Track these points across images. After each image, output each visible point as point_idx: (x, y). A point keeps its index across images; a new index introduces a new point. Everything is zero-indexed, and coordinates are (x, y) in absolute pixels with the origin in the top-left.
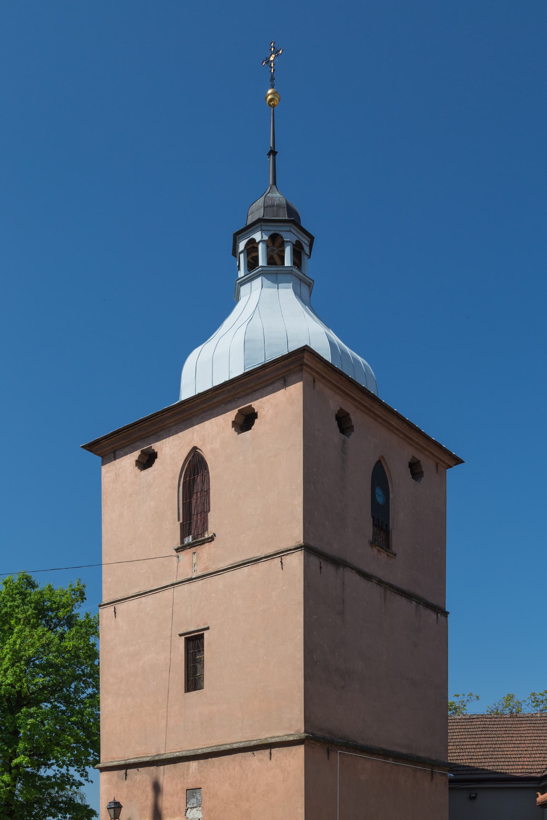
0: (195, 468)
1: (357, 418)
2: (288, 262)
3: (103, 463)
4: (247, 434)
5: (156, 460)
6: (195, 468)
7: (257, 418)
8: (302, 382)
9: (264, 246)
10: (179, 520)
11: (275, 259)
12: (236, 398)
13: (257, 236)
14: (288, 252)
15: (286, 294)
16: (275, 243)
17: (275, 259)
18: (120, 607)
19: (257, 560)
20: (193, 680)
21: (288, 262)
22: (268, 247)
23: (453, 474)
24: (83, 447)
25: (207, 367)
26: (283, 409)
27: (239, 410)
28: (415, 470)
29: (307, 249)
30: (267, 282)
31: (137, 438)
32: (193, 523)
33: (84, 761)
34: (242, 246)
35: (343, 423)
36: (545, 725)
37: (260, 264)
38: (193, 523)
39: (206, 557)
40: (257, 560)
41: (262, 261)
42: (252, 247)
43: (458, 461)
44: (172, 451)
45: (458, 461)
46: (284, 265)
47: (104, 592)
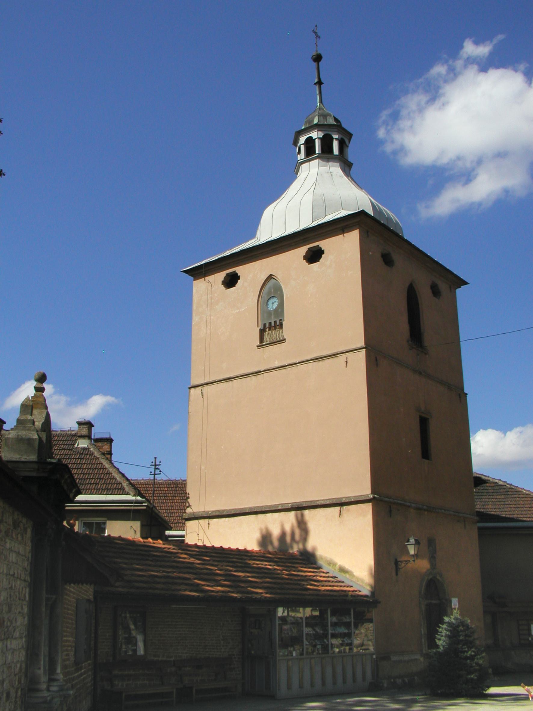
0: (271, 288)
1: (397, 257)
2: (336, 151)
3: (194, 280)
4: (315, 265)
5: (239, 281)
6: (271, 288)
7: (324, 254)
8: (358, 230)
9: (320, 141)
10: (258, 326)
11: (327, 149)
12: (309, 241)
14: (335, 144)
15: (336, 169)
16: (327, 142)
17: (327, 149)
18: (206, 389)
19: (258, 373)
20: (426, 454)
21: (336, 151)
23: (460, 292)
25: (281, 218)
26: (345, 249)
27: (253, 235)
28: (436, 291)
30: (322, 163)
31: (227, 268)
32: (271, 328)
33: (74, 491)
34: (302, 140)
35: (387, 260)
36: (530, 509)
37: (317, 152)
38: (271, 328)
39: (274, 355)
40: (258, 373)
41: (318, 150)
42: (310, 142)
43: (465, 283)
44: (252, 274)
45: (465, 283)
47: (193, 375)
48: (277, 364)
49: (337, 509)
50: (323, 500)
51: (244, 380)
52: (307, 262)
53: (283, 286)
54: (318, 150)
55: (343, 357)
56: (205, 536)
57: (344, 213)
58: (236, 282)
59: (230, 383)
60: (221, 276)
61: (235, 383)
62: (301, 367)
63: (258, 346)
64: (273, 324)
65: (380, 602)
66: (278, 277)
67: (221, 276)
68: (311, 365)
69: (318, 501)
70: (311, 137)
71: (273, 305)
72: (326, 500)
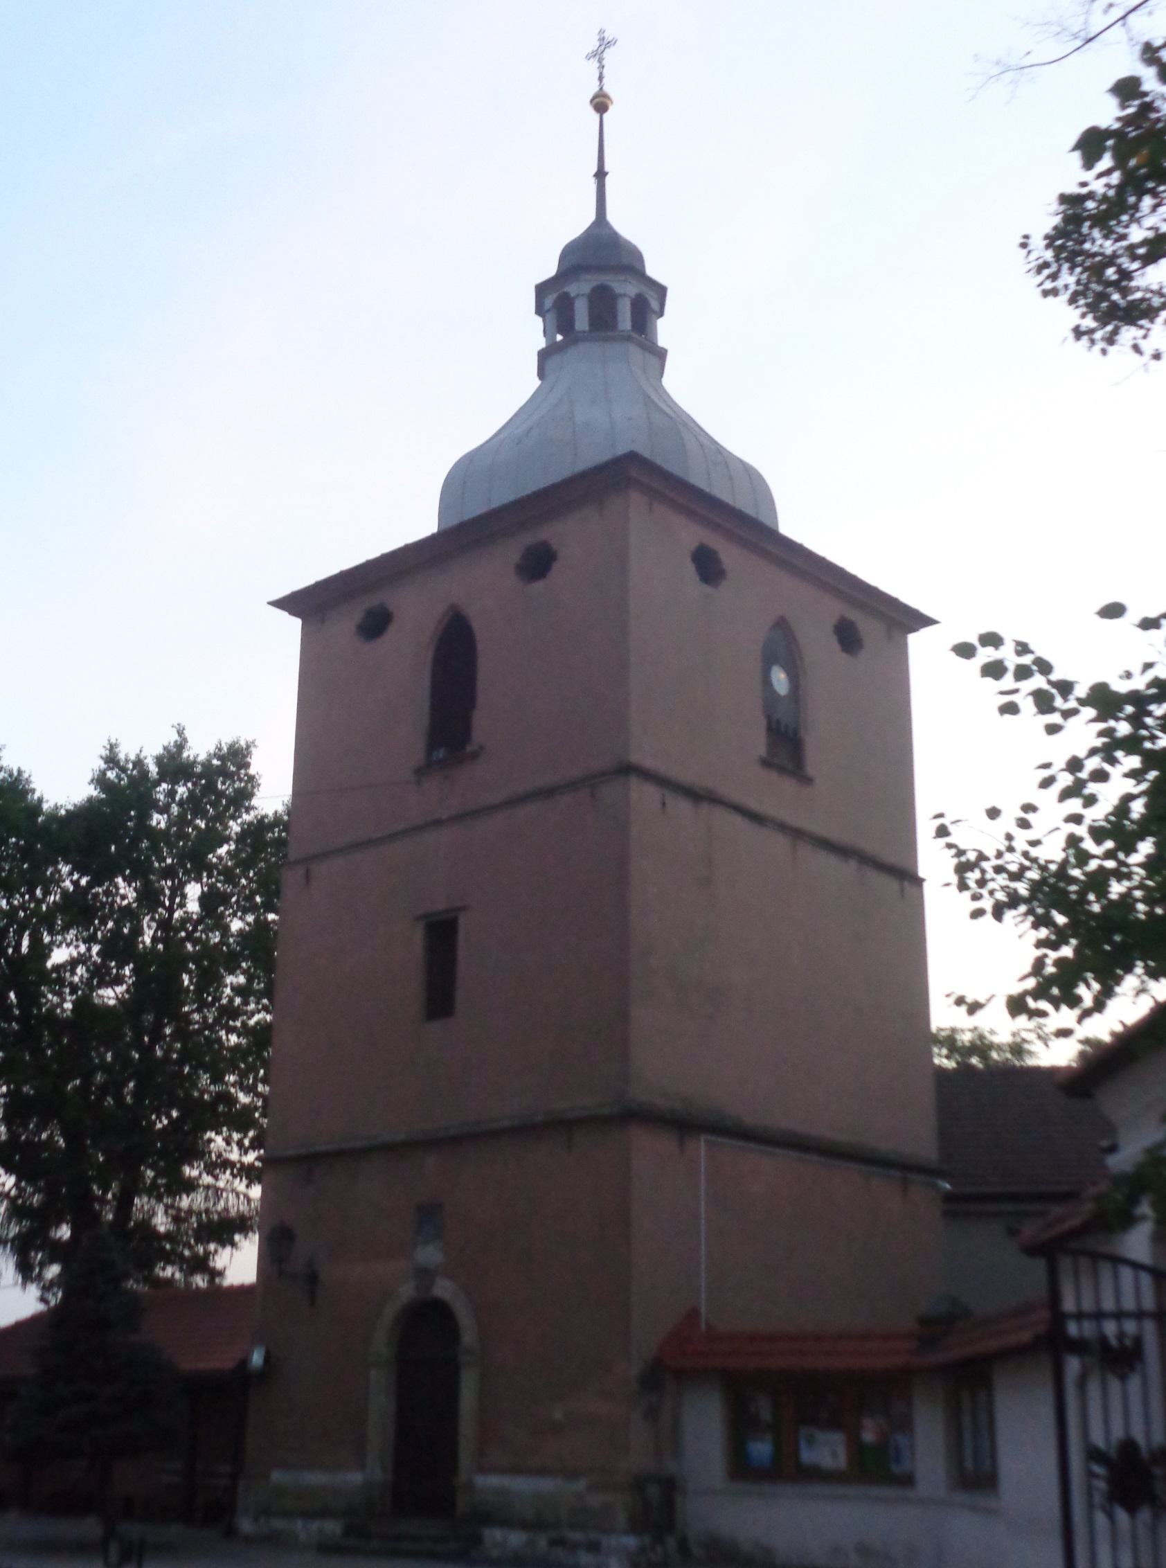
1: (729, 555)
4: (539, 586)
24: (281, 604)
28: (848, 638)
29: (655, 305)
34: (549, 302)
35: (708, 567)
41: (582, 321)
43: (927, 621)
54: (582, 321)
60: (510, 552)
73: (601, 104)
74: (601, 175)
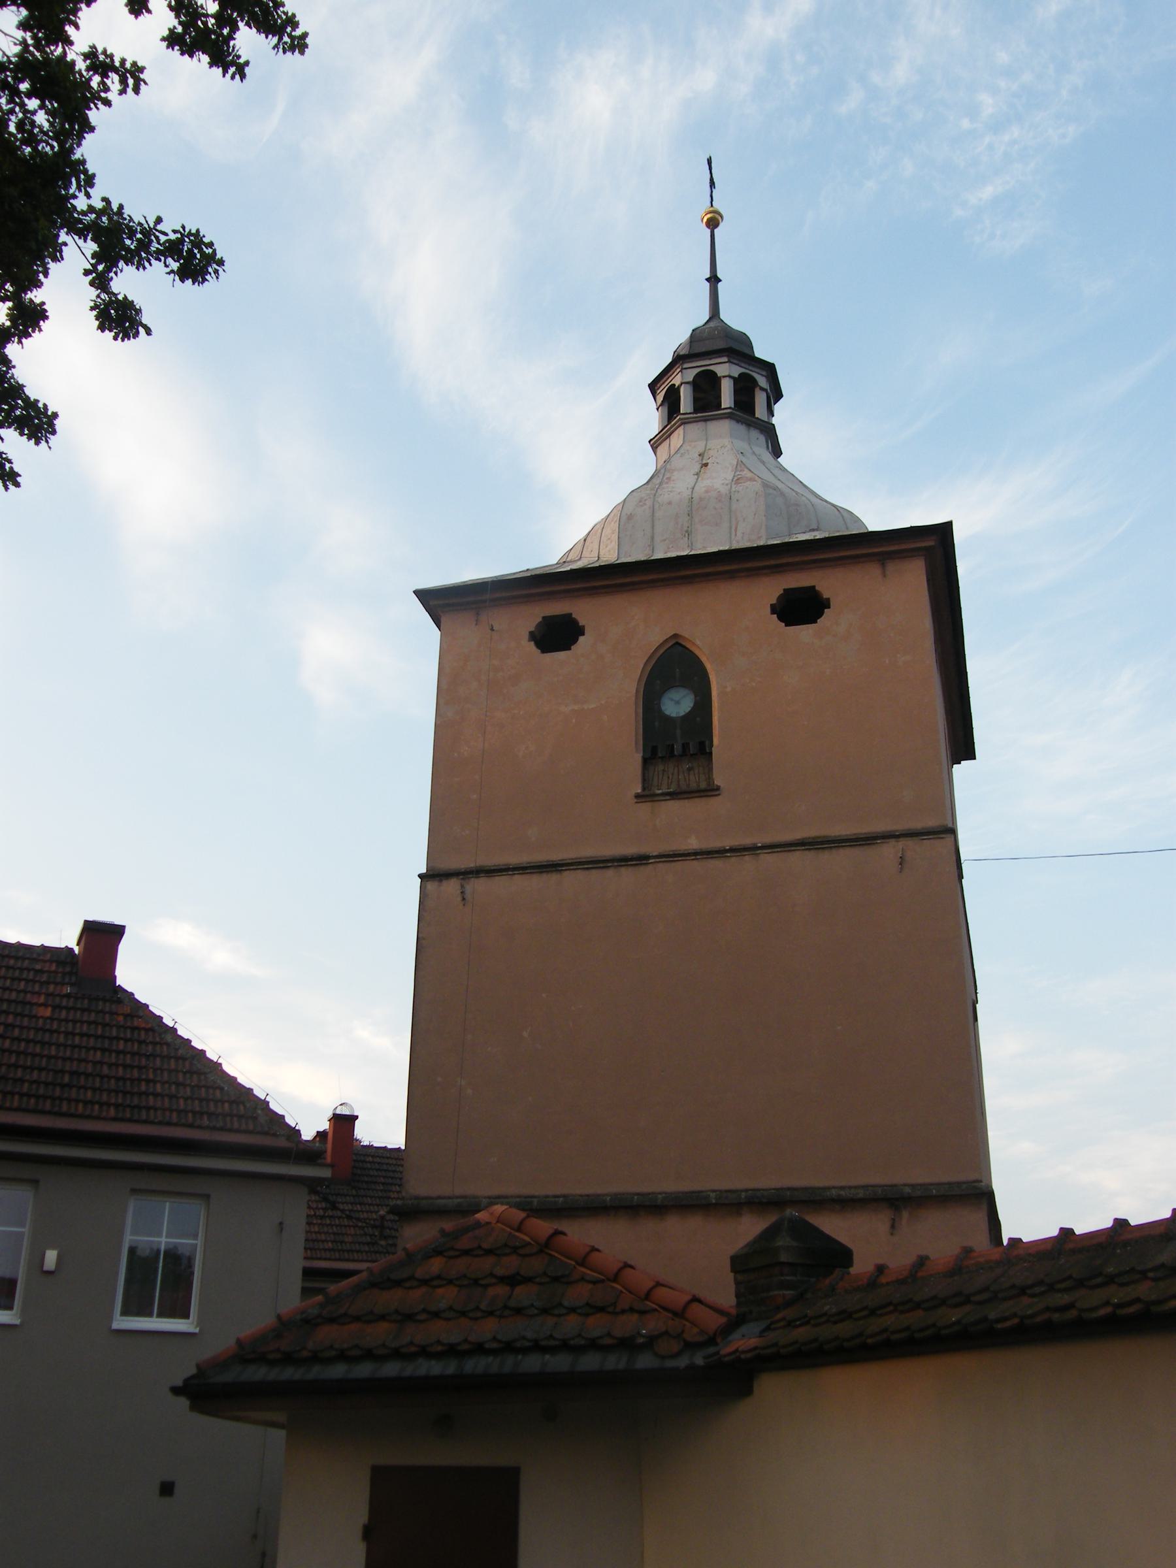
0: (676, 666)
4: (804, 633)
6: (676, 666)
13: (677, 381)
16: (706, 386)
18: (478, 886)
19: (641, 860)
22: (694, 390)
24: (420, 594)
39: (681, 823)
40: (641, 860)
41: (727, 399)
43: (420, 594)
46: (753, 413)
48: (693, 844)
49: (701, 424)
50: (842, 1188)
51: (595, 875)
52: (780, 619)
53: (708, 666)
54: (727, 399)
55: (889, 851)
56: (457, 1253)
57: (818, 535)
58: (575, 641)
59: (554, 877)
60: (771, 589)
61: (571, 879)
62: (768, 860)
63: (637, 796)
64: (678, 749)
65: (357, 1117)
66: (698, 642)
67: (771, 589)
68: (797, 859)
69: (829, 1188)
70: (714, 374)
71: (678, 704)
72: (856, 1187)
73: (713, 223)
74: (714, 280)
